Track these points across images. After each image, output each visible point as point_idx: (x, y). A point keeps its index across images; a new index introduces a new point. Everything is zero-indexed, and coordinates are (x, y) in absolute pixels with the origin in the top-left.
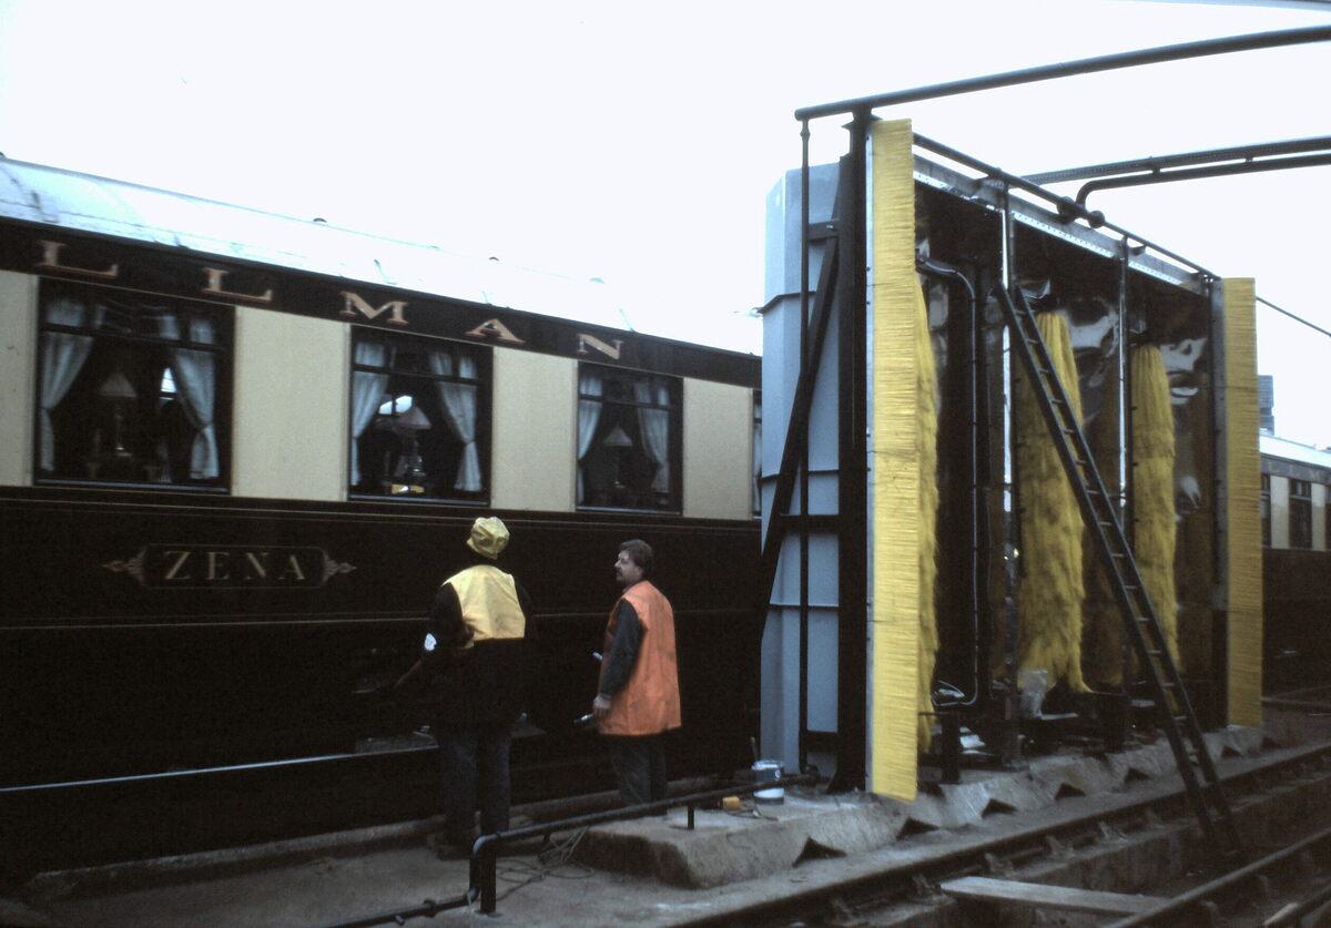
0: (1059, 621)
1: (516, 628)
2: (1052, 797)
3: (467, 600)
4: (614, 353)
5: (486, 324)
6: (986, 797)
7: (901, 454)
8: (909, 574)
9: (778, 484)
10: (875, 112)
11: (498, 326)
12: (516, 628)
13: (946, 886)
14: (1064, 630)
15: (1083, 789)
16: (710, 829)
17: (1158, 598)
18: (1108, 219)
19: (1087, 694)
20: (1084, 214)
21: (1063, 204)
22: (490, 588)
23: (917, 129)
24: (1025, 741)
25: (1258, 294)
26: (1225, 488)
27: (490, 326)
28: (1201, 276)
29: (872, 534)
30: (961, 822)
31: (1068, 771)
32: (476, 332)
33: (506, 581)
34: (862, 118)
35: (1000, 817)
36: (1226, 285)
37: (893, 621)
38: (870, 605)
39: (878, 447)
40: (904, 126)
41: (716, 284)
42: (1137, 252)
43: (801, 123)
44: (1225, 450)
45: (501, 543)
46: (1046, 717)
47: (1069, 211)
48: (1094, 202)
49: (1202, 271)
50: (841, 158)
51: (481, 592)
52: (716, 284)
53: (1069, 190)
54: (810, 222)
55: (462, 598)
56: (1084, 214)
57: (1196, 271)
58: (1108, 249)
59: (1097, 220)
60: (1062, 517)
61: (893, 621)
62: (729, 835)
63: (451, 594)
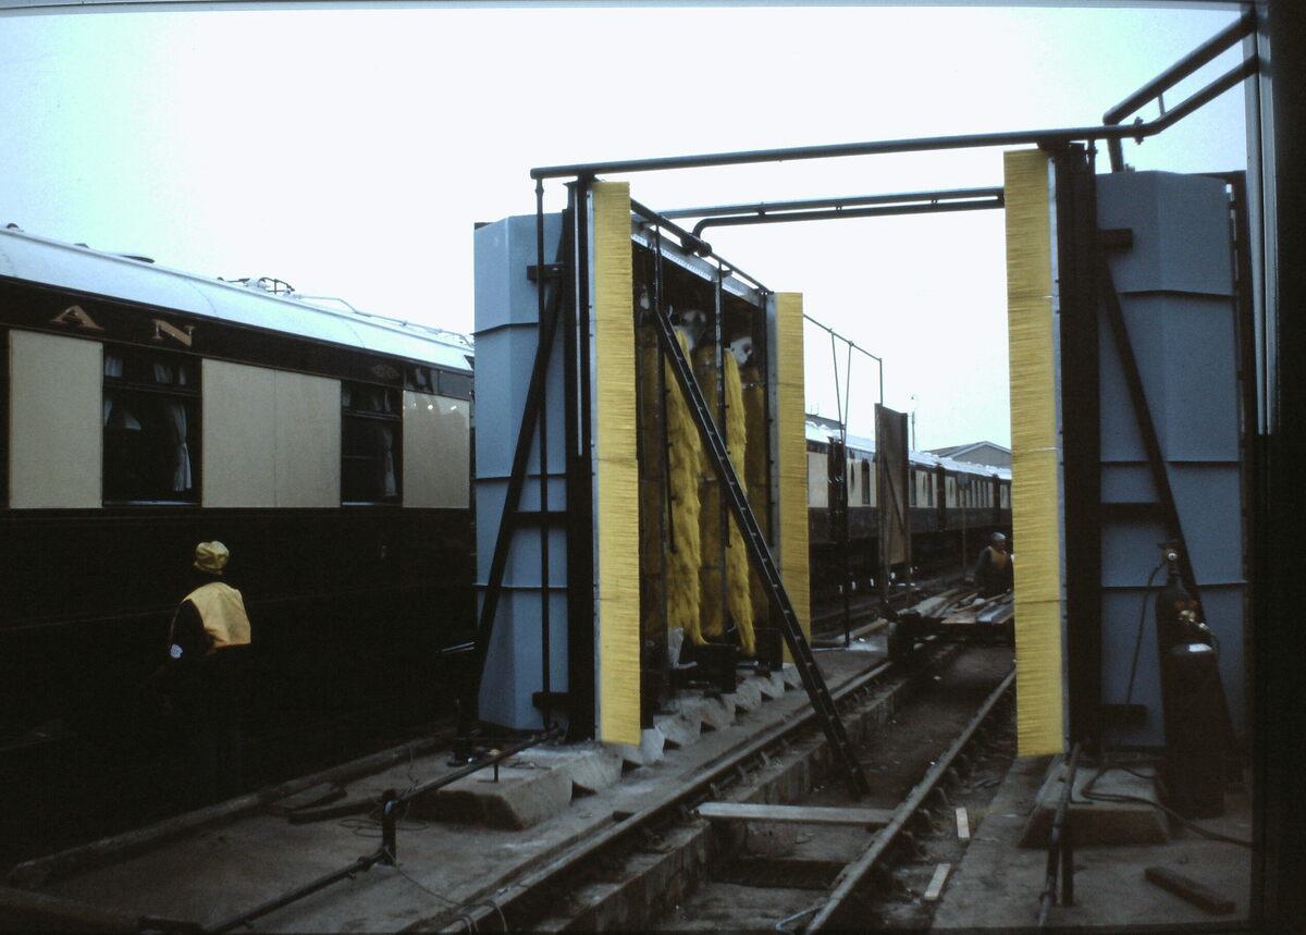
0: (685, 587)
1: (245, 637)
2: (698, 732)
3: (207, 613)
4: (187, 340)
5: (68, 311)
6: (662, 737)
7: (622, 461)
8: (631, 560)
9: (510, 485)
10: (598, 177)
11: (79, 313)
12: (245, 637)
14: (688, 592)
16: (513, 781)
17: (736, 562)
18: (714, 251)
19: (705, 646)
22: (224, 600)
25: (805, 312)
26: (777, 468)
27: (72, 313)
28: (763, 294)
29: (597, 528)
30: (653, 760)
31: (702, 711)
32: (59, 319)
33: (235, 595)
34: (584, 180)
35: (672, 752)
36: (778, 299)
37: (617, 598)
38: (597, 586)
39: (601, 456)
41: (422, 300)
43: (535, 181)
44: (777, 437)
45: (222, 560)
46: (685, 667)
48: (707, 235)
51: (217, 607)
52: (422, 300)
53: (688, 225)
54: (545, 263)
55: (202, 611)
57: (755, 287)
58: (742, 291)
59: (706, 250)
60: (686, 500)
61: (617, 598)
62: (529, 784)
63: (191, 606)
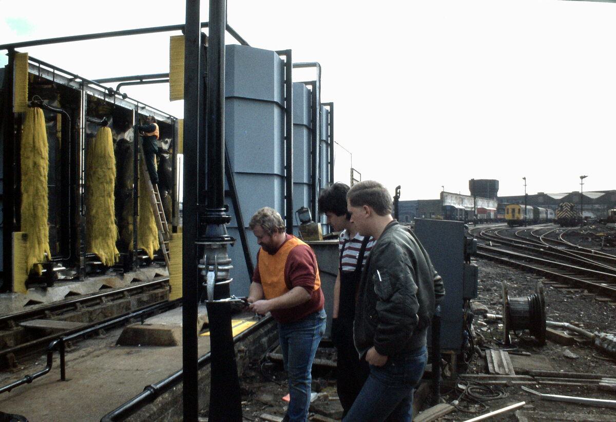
10: (16, 49)
13: (22, 324)
15: (112, 286)
18: (128, 96)
20: (119, 94)
21: (110, 90)
23: (30, 55)
24: (439, 280)
40: (25, 55)
42: (143, 108)
47: (111, 93)
49: (170, 116)
50: (372, 185)
53: (114, 86)
56: (119, 94)
59: (125, 96)
